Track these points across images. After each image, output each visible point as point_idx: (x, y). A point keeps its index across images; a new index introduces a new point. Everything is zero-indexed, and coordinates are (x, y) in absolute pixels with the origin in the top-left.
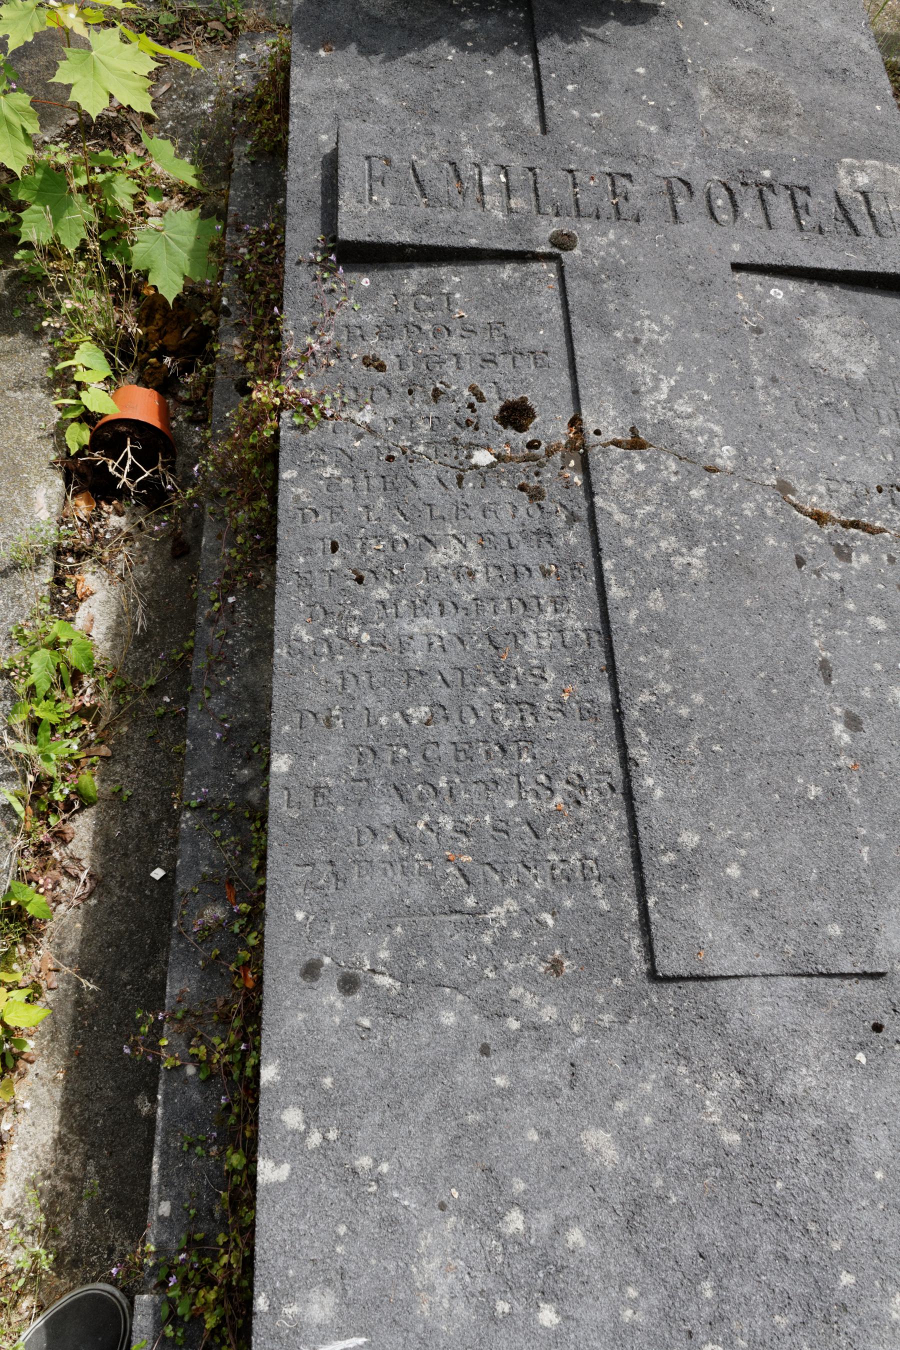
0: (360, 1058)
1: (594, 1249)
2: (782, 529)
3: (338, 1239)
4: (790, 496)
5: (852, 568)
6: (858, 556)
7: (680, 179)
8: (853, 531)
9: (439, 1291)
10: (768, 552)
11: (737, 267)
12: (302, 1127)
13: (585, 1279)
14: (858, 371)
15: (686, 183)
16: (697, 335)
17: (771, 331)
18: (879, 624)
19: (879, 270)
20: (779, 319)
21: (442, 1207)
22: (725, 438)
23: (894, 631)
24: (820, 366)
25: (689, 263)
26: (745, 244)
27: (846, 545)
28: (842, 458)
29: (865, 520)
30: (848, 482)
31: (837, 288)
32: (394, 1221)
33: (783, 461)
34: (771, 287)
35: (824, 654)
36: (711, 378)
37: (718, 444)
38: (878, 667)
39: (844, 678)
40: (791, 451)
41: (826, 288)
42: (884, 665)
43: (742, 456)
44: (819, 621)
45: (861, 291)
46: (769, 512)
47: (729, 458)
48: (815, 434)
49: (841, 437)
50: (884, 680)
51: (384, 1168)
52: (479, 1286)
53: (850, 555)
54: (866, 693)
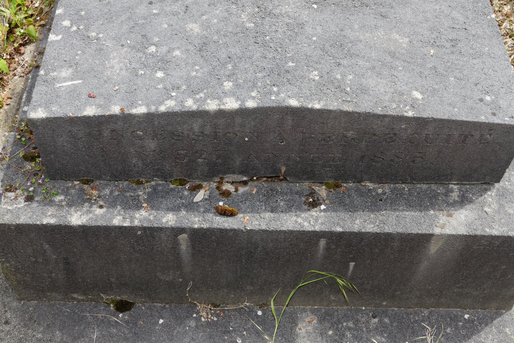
0: (97, 7)
1: (184, 56)
3: (77, 55)
9: (116, 68)
12: (70, 25)
13: (178, 64)
21: (122, 46)
32: (101, 50)
51: (101, 35)
52: (133, 66)
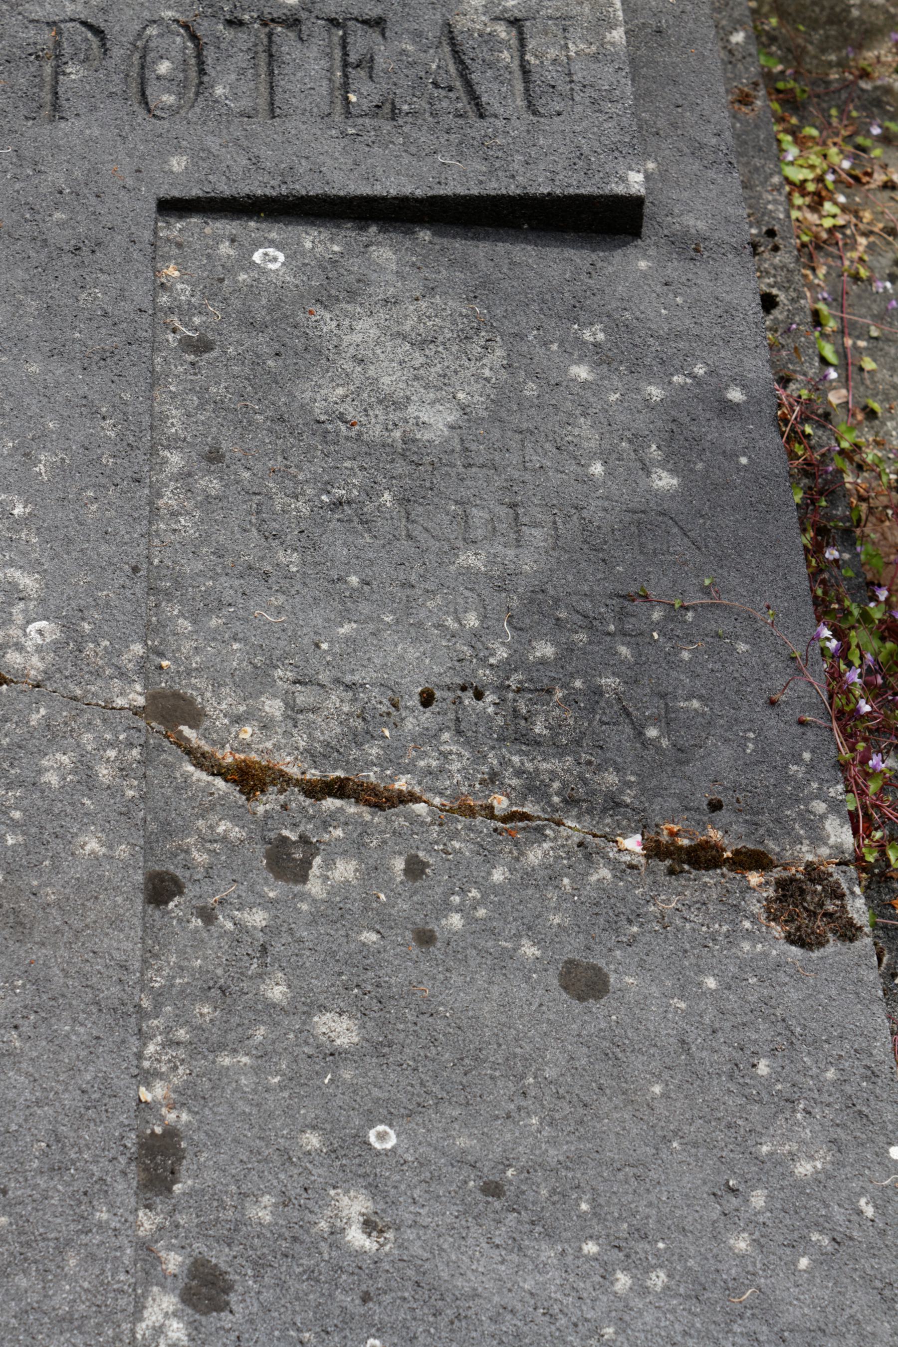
2: (126, 814)
4: (186, 730)
5: (303, 896)
6: (329, 864)
7: (84, 23)
8: (331, 803)
10: (77, 872)
11: (171, 207)
14: (435, 420)
15: (98, 32)
16: (34, 368)
17: (234, 343)
18: (340, 1029)
19: (513, 190)
20: (262, 315)
22: (42, 601)
23: (377, 1046)
24: (341, 418)
25: (57, 206)
26: (201, 154)
27: (304, 840)
28: (345, 629)
29: (372, 776)
30: (348, 687)
31: (425, 235)
33: (187, 646)
34: (257, 245)
35: (171, 1117)
36: (43, 465)
37: (19, 618)
38: (312, 1140)
39: (210, 1176)
40: (214, 622)
41: (397, 237)
42: (326, 1134)
43: (72, 641)
44: (182, 1034)
45: (486, 237)
46: (104, 773)
47: (39, 649)
48: (290, 577)
49: (354, 580)
50: (319, 1174)
53: (307, 864)
54: (262, 1212)
